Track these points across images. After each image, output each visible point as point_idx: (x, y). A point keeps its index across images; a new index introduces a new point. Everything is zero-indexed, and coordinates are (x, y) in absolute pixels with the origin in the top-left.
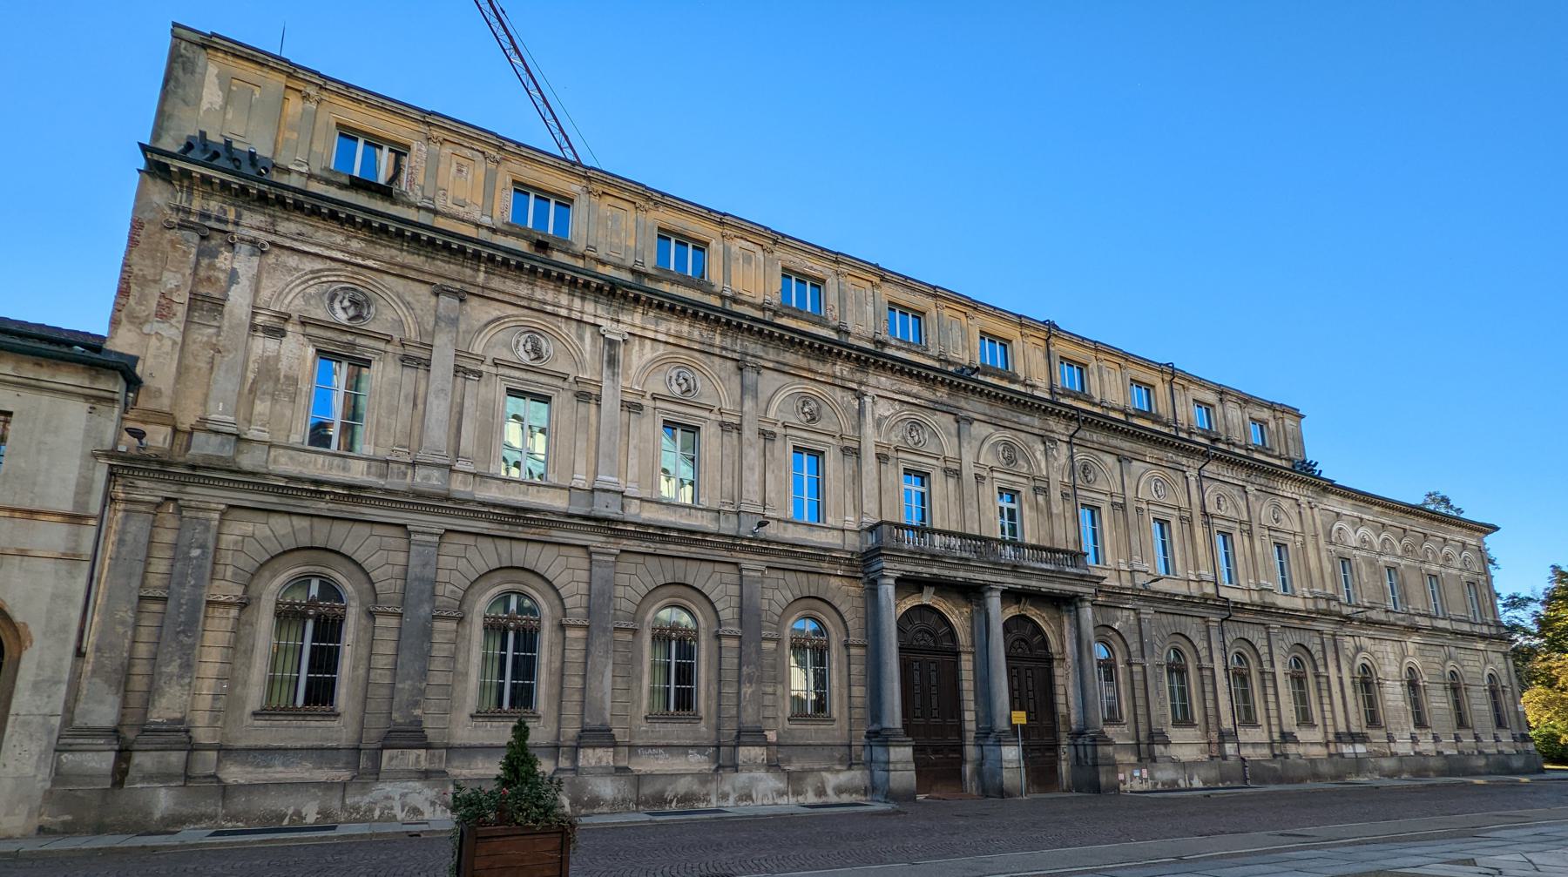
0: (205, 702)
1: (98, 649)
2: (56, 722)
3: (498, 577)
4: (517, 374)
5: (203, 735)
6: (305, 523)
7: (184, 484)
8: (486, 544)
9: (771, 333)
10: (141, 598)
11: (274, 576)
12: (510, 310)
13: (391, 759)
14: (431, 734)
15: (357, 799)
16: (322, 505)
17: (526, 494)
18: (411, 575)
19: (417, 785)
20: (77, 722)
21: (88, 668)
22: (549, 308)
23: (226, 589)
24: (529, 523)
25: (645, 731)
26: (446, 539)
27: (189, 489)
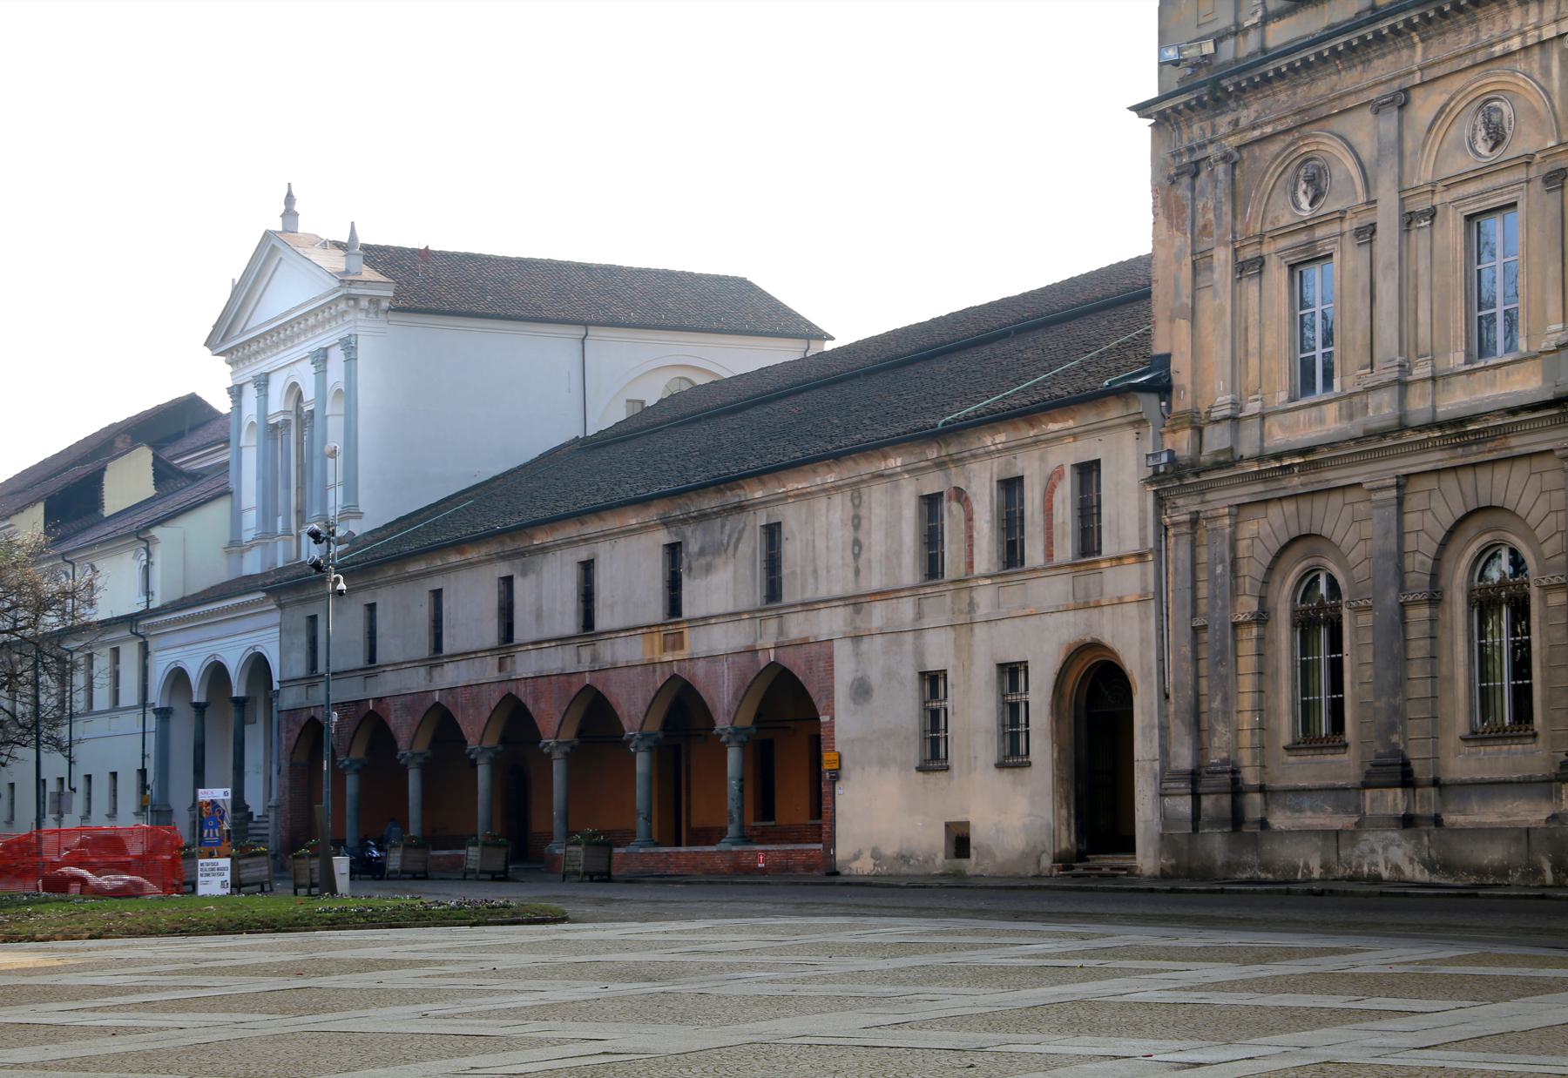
0: (1246, 739)
1: (1176, 690)
2: (1157, 765)
3: (1472, 527)
4: (1471, 188)
5: (1250, 777)
6: (1289, 507)
7: (1202, 493)
8: (1449, 482)
9: (1305, 61)
10: (1194, 629)
11: (1284, 579)
12: (1458, 82)
13: (1373, 800)
14: (1420, 770)
15: (1349, 851)
16: (1296, 481)
17: (1492, 384)
18: (611, 673)
19: (1394, 835)
20: (1173, 766)
21: (1172, 709)
22: (1498, 49)
23: (1248, 605)
24: (1482, 437)
25: (1461, 764)
26: (1409, 489)
27: (1209, 497)
